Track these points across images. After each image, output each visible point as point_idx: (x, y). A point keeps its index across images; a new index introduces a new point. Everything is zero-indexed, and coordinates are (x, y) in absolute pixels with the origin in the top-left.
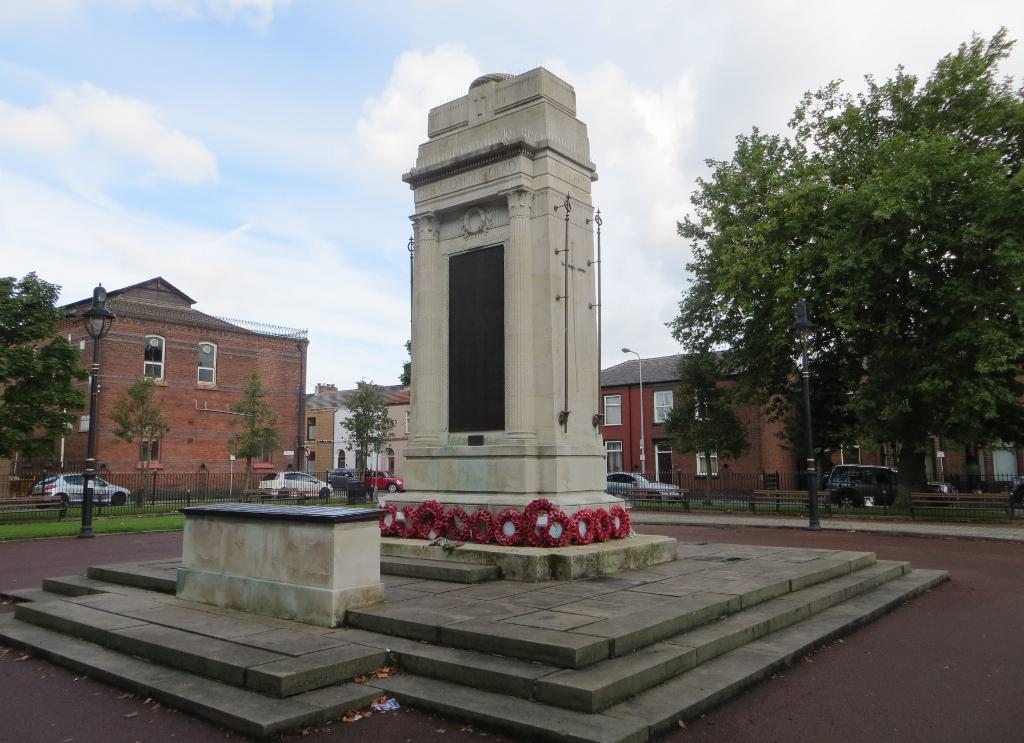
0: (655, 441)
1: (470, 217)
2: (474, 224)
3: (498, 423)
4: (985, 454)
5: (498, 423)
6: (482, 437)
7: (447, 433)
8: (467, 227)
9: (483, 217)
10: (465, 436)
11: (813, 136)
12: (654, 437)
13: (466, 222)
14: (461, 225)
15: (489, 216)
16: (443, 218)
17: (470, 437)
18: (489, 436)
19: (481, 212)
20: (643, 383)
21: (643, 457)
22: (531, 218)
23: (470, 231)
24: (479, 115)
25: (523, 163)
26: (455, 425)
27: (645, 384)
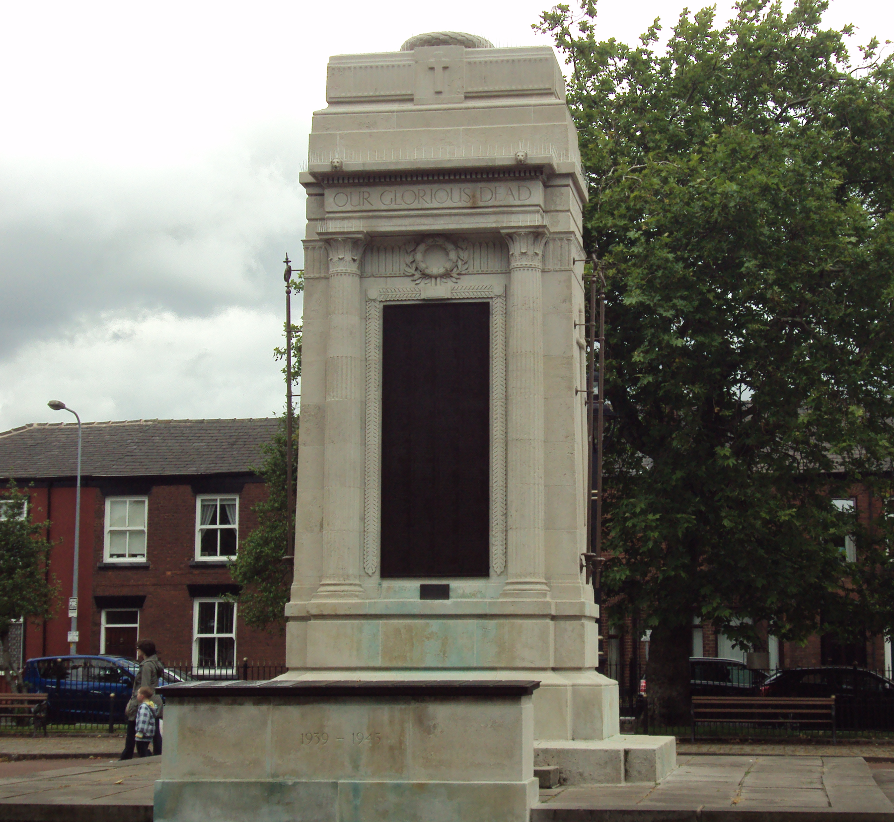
0: (102, 602)
1: (426, 251)
2: (436, 264)
3: (479, 567)
4: (705, 638)
5: (479, 567)
6: (448, 586)
7: (188, 583)
8: (422, 266)
9: (453, 255)
10: (413, 586)
11: (555, 50)
12: (100, 593)
13: (419, 256)
14: (410, 259)
15: (464, 255)
16: (371, 246)
17: (423, 587)
18: (459, 586)
19: (450, 247)
20: (83, 478)
21: (73, 636)
22: (543, 271)
23: (428, 271)
24: (439, 93)
25: (536, 194)
26: (392, 567)
27: (88, 481)
